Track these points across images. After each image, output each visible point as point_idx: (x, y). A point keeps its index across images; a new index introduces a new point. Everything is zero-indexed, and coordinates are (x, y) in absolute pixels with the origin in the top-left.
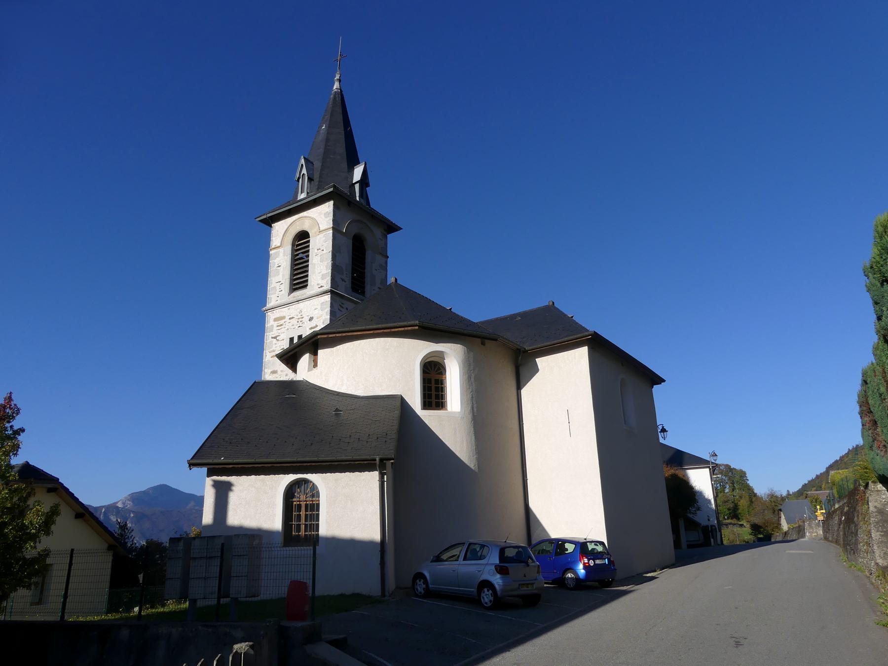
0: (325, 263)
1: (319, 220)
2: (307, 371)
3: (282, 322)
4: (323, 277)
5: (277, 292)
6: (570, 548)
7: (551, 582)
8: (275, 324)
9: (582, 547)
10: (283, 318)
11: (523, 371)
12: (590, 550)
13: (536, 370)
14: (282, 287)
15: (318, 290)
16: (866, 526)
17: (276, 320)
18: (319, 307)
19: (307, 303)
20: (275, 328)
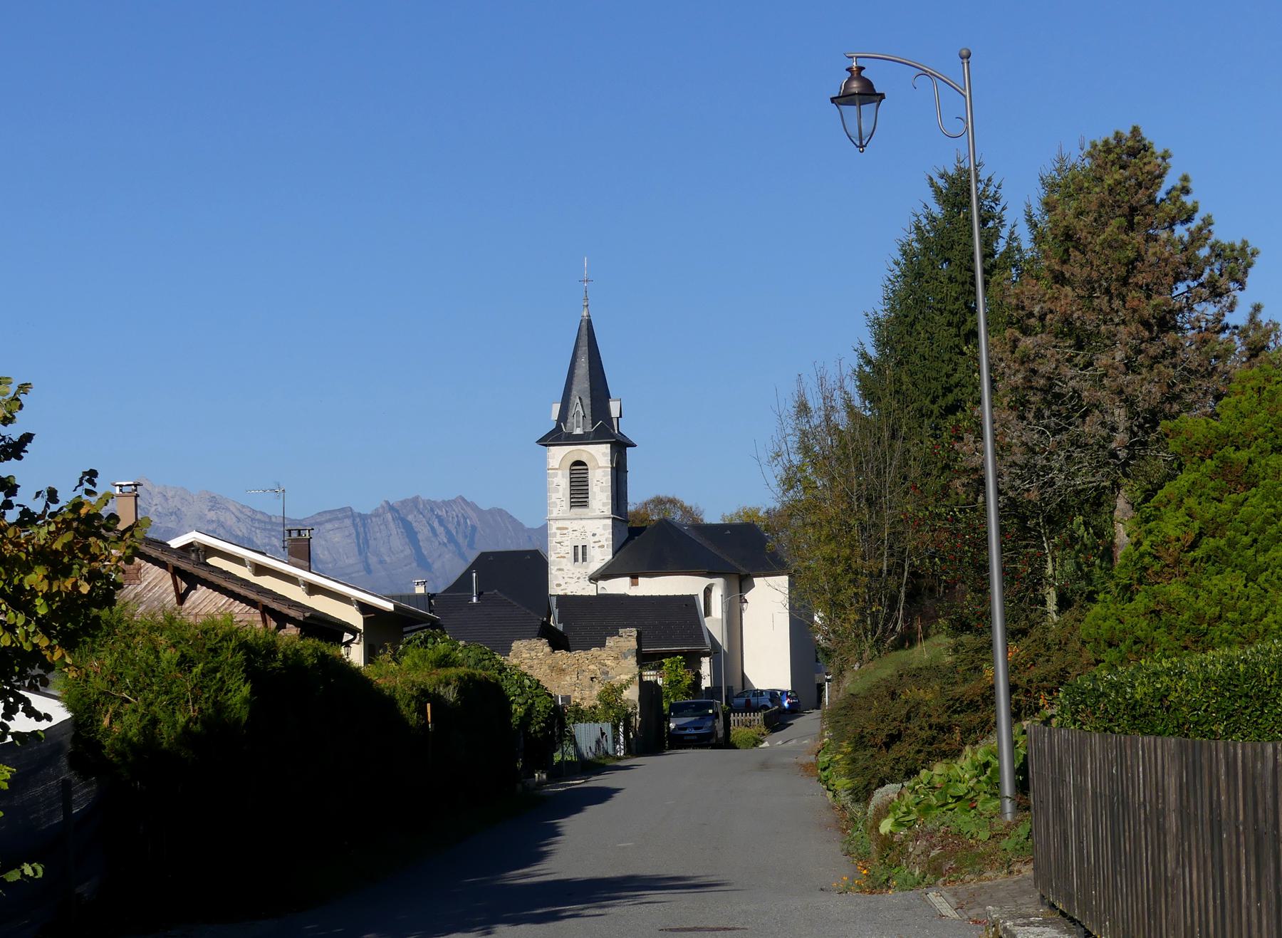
0: (606, 494)
1: (597, 457)
2: (622, 639)
3: (565, 532)
4: (604, 504)
5: (559, 507)
6: (779, 693)
7: (429, 624)
8: (559, 532)
9: (783, 692)
10: (567, 529)
11: (743, 584)
12: (703, 688)
13: (753, 586)
14: (563, 503)
15: (598, 513)
16: (175, 689)
17: (558, 529)
18: (601, 527)
19: (590, 521)
20: (558, 535)
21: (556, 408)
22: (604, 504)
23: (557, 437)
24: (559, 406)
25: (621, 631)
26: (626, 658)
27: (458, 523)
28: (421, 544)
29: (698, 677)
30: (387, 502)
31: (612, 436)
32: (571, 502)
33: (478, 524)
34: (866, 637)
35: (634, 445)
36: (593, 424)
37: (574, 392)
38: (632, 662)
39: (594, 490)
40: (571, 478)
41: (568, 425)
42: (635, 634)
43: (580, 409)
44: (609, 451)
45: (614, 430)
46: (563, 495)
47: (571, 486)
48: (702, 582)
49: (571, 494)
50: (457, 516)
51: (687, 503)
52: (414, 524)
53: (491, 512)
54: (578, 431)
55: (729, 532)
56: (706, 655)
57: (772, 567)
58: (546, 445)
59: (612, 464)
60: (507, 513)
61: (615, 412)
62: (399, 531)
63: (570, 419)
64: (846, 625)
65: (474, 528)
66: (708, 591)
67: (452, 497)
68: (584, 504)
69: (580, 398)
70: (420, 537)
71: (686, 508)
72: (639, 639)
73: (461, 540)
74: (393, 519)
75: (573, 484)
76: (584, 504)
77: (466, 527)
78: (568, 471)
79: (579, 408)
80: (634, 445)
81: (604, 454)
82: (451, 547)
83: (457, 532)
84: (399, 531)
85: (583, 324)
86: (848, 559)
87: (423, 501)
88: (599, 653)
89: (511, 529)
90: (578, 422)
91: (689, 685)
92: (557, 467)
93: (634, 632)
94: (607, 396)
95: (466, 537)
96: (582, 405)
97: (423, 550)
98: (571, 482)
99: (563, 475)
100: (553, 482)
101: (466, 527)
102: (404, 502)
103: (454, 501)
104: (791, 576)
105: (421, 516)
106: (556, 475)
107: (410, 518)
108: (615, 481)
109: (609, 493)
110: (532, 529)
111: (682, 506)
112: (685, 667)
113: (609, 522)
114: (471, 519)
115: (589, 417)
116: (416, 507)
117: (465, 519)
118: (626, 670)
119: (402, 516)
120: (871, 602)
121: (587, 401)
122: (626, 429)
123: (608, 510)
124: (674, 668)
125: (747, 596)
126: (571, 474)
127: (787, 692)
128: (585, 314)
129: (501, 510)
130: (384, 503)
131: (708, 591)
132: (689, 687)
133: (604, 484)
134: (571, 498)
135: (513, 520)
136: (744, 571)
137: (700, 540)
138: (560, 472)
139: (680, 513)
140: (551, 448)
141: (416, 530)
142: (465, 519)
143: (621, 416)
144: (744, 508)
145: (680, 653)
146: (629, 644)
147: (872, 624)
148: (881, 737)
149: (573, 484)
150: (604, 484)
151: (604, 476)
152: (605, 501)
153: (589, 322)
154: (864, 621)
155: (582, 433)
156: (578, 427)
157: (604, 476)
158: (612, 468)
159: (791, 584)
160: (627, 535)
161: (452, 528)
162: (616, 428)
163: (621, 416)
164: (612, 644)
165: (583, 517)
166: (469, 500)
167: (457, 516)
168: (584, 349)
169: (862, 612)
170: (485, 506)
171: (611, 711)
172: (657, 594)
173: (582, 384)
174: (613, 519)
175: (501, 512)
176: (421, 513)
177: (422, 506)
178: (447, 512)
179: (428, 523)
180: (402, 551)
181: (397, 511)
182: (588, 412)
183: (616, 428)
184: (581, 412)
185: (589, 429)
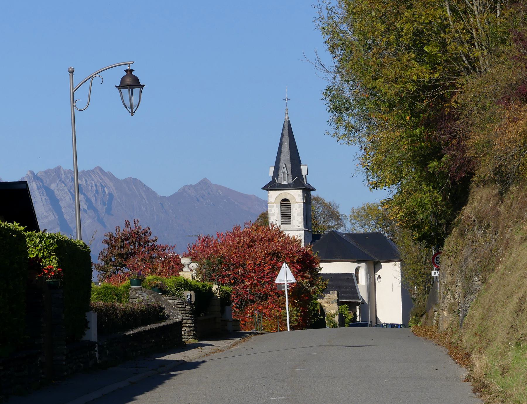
2: (331, 295)
4: (300, 223)
13: (381, 267)
15: (296, 227)
21: (272, 170)
22: (300, 223)
23: (273, 186)
24: (273, 168)
25: (331, 292)
26: (333, 303)
27: (97, 191)
28: (63, 210)
29: (355, 315)
30: (32, 172)
31: (303, 185)
32: (281, 221)
33: (115, 194)
34: (426, 294)
35: (315, 190)
36: (293, 179)
37: (282, 161)
38: (336, 304)
39: (294, 215)
40: (281, 208)
41: (279, 179)
42: (336, 293)
43: (285, 170)
44: (302, 193)
45: (304, 182)
46: (277, 217)
47: (281, 212)
48: (355, 265)
49: (281, 217)
50: (96, 185)
51: (327, 201)
52: (56, 192)
53: (125, 181)
54: (285, 183)
55: (367, 237)
56: (358, 305)
57: (392, 257)
58: (267, 190)
59: (303, 200)
60: (141, 182)
61: (304, 172)
62: (43, 198)
63: (280, 176)
64: (420, 290)
65: (111, 195)
66: (357, 270)
67: (92, 168)
68: (289, 222)
69: (285, 165)
70: (62, 204)
71: (326, 204)
72: (338, 295)
73: (99, 206)
74: (38, 188)
75: (282, 211)
76: (289, 222)
77: (104, 195)
78: (279, 205)
79: (285, 170)
80: (315, 190)
81: (299, 195)
82: (91, 213)
83: (96, 200)
84: (43, 198)
85: (285, 123)
86: (419, 270)
87: (65, 171)
88: (322, 301)
89: (145, 197)
90: (284, 177)
91: (350, 319)
92: (274, 202)
93: (336, 292)
94: (300, 163)
95: (104, 204)
96: (286, 168)
97: (65, 216)
98: (281, 210)
99: (276, 206)
100: (271, 210)
101: (104, 195)
102: (47, 172)
103: (92, 171)
104: (402, 261)
105: (63, 185)
106: (273, 206)
107: (53, 187)
108: (305, 211)
109: (302, 217)
110: (165, 197)
111: (323, 202)
112: (349, 310)
113: (303, 232)
114: (108, 188)
115: (290, 175)
116: (59, 177)
117: (103, 187)
118: (333, 308)
119: (45, 185)
120: (427, 283)
121: (289, 166)
122: (310, 181)
123: (302, 226)
124: (343, 310)
125: (379, 273)
126: (281, 206)
127: (400, 325)
128: (287, 118)
129: (136, 179)
130: (29, 173)
131: (357, 270)
132: (351, 320)
133: (299, 212)
134: (281, 219)
135: (148, 190)
136: (376, 259)
137: (352, 242)
138: (275, 205)
139: (322, 207)
140: (270, 191)
141: (58, 198)
142: (103, 187)
143: (307, 174)
144: (368, 204)
145: (346, 303)
146: (334, 297)
147: (428, 290)
148: (421, 314)
149: (282, 211)
150: (299, 212)
151: (299, 207)
152: (300, 221)
153: (289, 122)
154: (425, 289)
155: (287, 183)
156: (285, 180)
157: (299, 207)
158: (304, 203)
159: (402, 266)
160: (312, 239)
161: (91, 195)
162: (305, 181)
163: (307, 174)
164: (327, 297)
165: (288, 229)
166: (106, 171)
167: (96, 185)
168: (286, 138)
169: (424, 286)
170: (121, 176)
171: (331, 323)
172: (337, 273)
173: (286, 157)
174: (305, 230)
175: (135, 182)
176: (63, 182)
177: (63, 176)
178: (86, 181)
179: (69, 191)
180: (46, 217)
181: (41, 181)
182: (290, 172)
183: (305, 181)
184: (286, 172)
185: (291, 181)
